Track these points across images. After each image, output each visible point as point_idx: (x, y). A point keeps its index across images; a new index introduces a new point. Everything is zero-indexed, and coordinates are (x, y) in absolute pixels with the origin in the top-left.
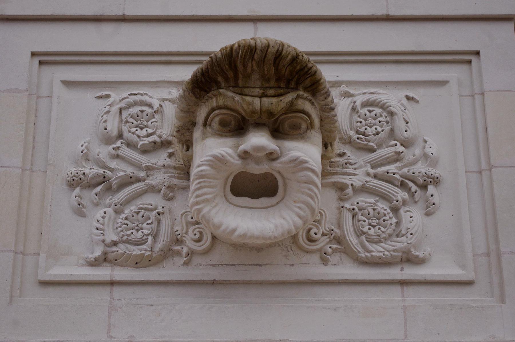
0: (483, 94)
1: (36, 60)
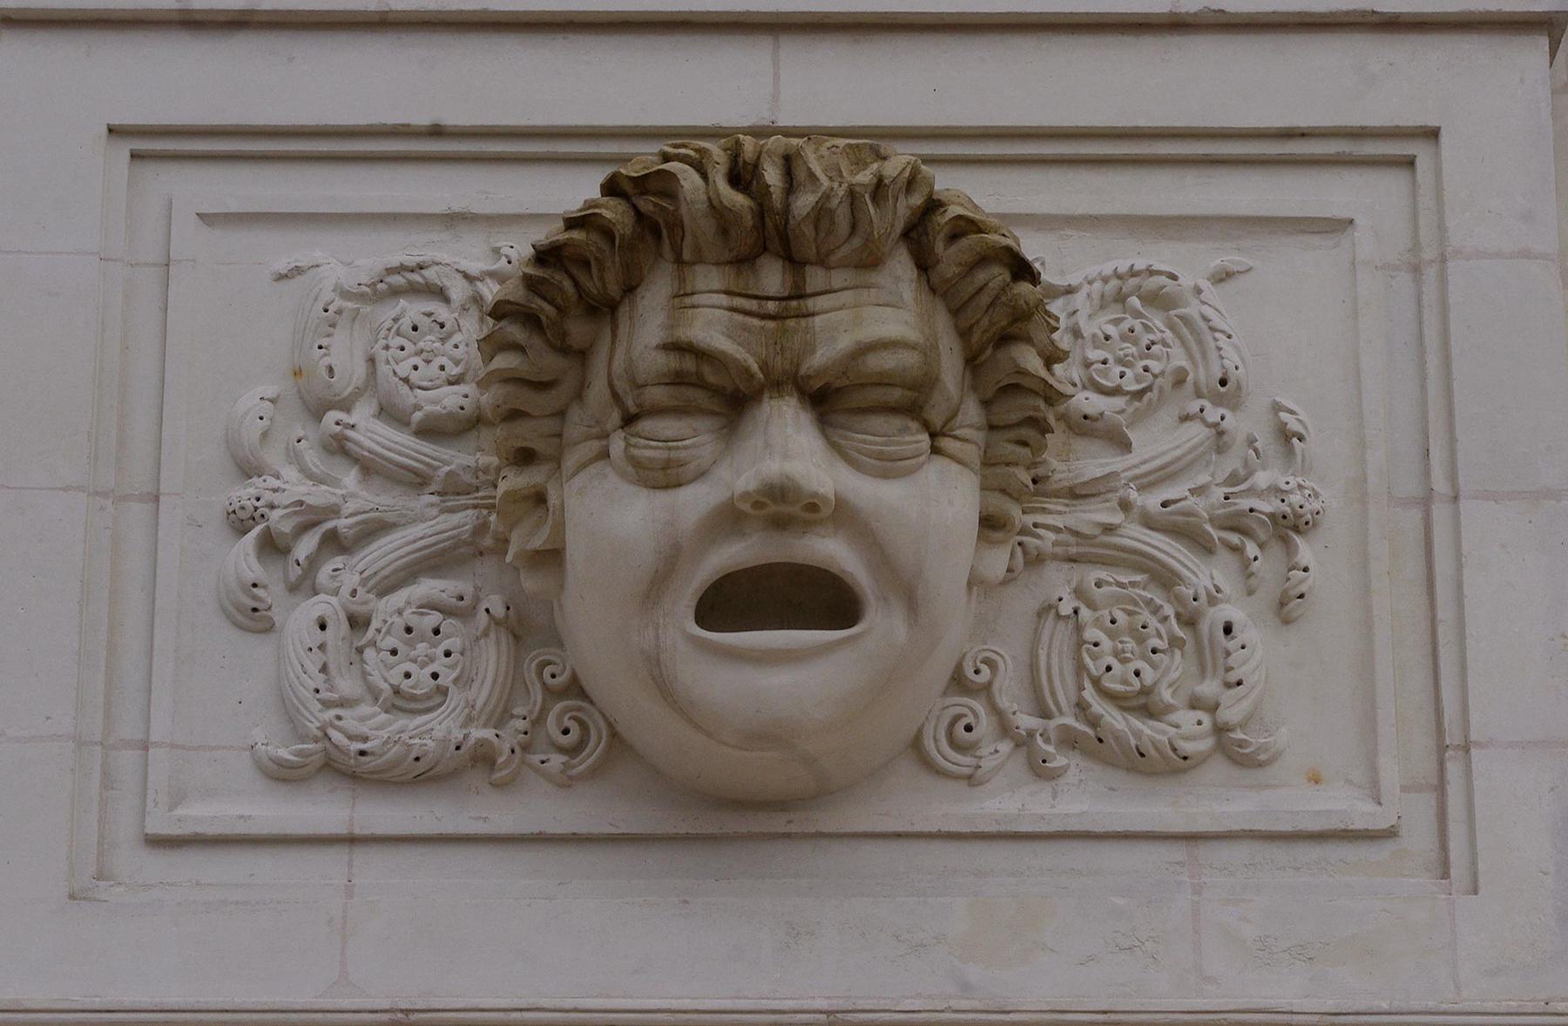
0: (1443, 260)
1: (125, 147)
